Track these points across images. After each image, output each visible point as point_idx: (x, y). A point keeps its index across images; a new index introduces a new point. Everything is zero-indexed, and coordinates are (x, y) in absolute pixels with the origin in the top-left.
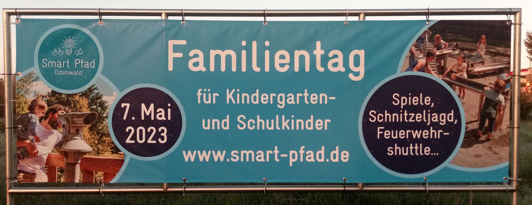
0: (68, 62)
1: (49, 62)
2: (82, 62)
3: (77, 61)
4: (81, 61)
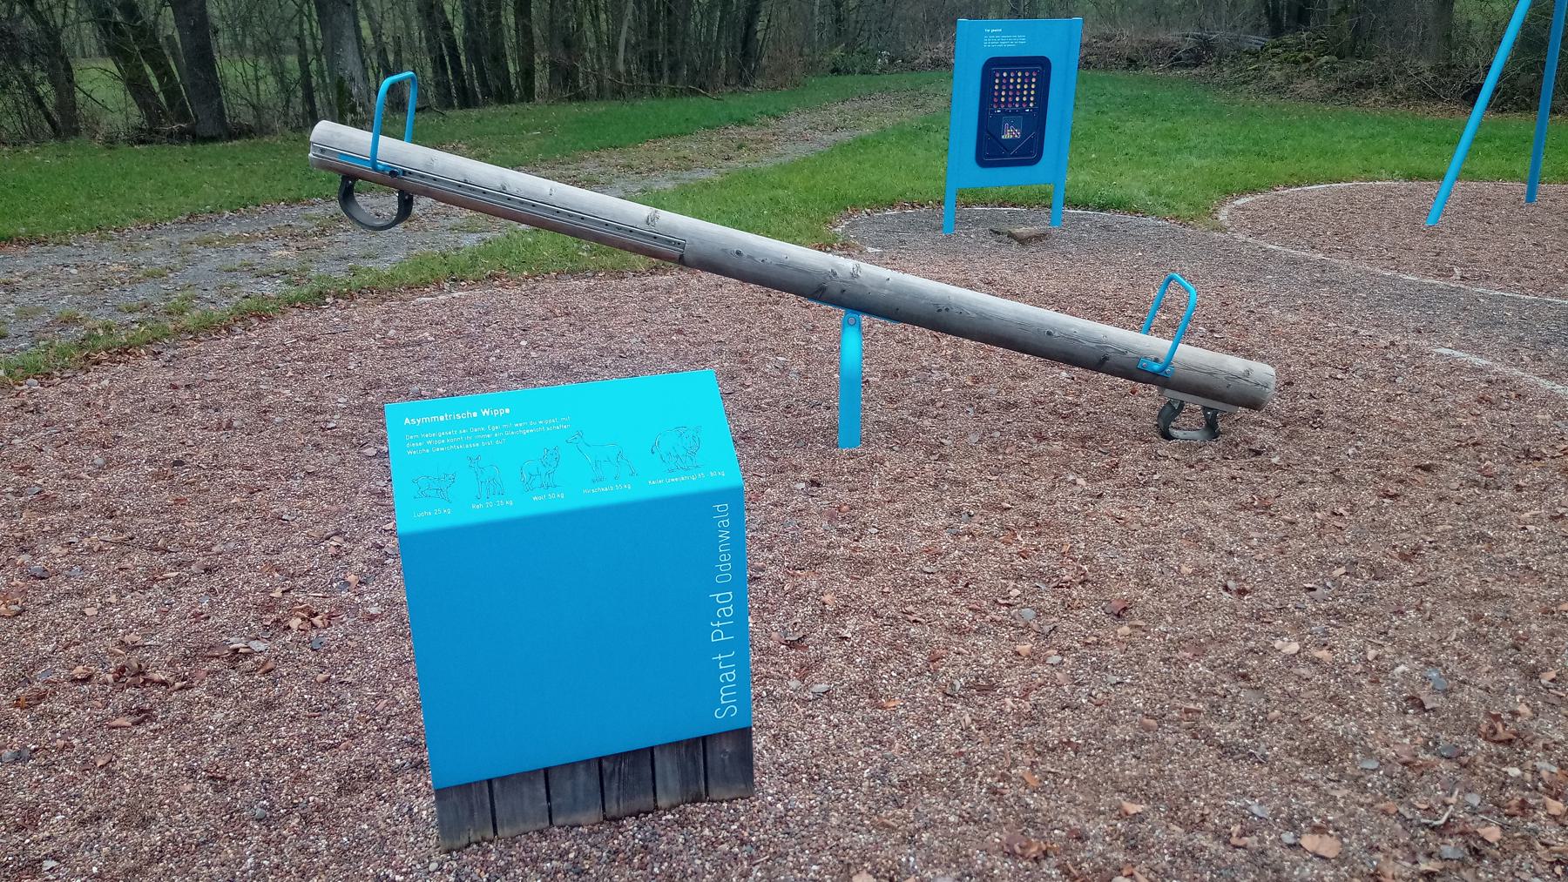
0: (720, 657)
1: (723, 702)
2: (718, 624)
3: (717, 635)
4: (716, 628)
